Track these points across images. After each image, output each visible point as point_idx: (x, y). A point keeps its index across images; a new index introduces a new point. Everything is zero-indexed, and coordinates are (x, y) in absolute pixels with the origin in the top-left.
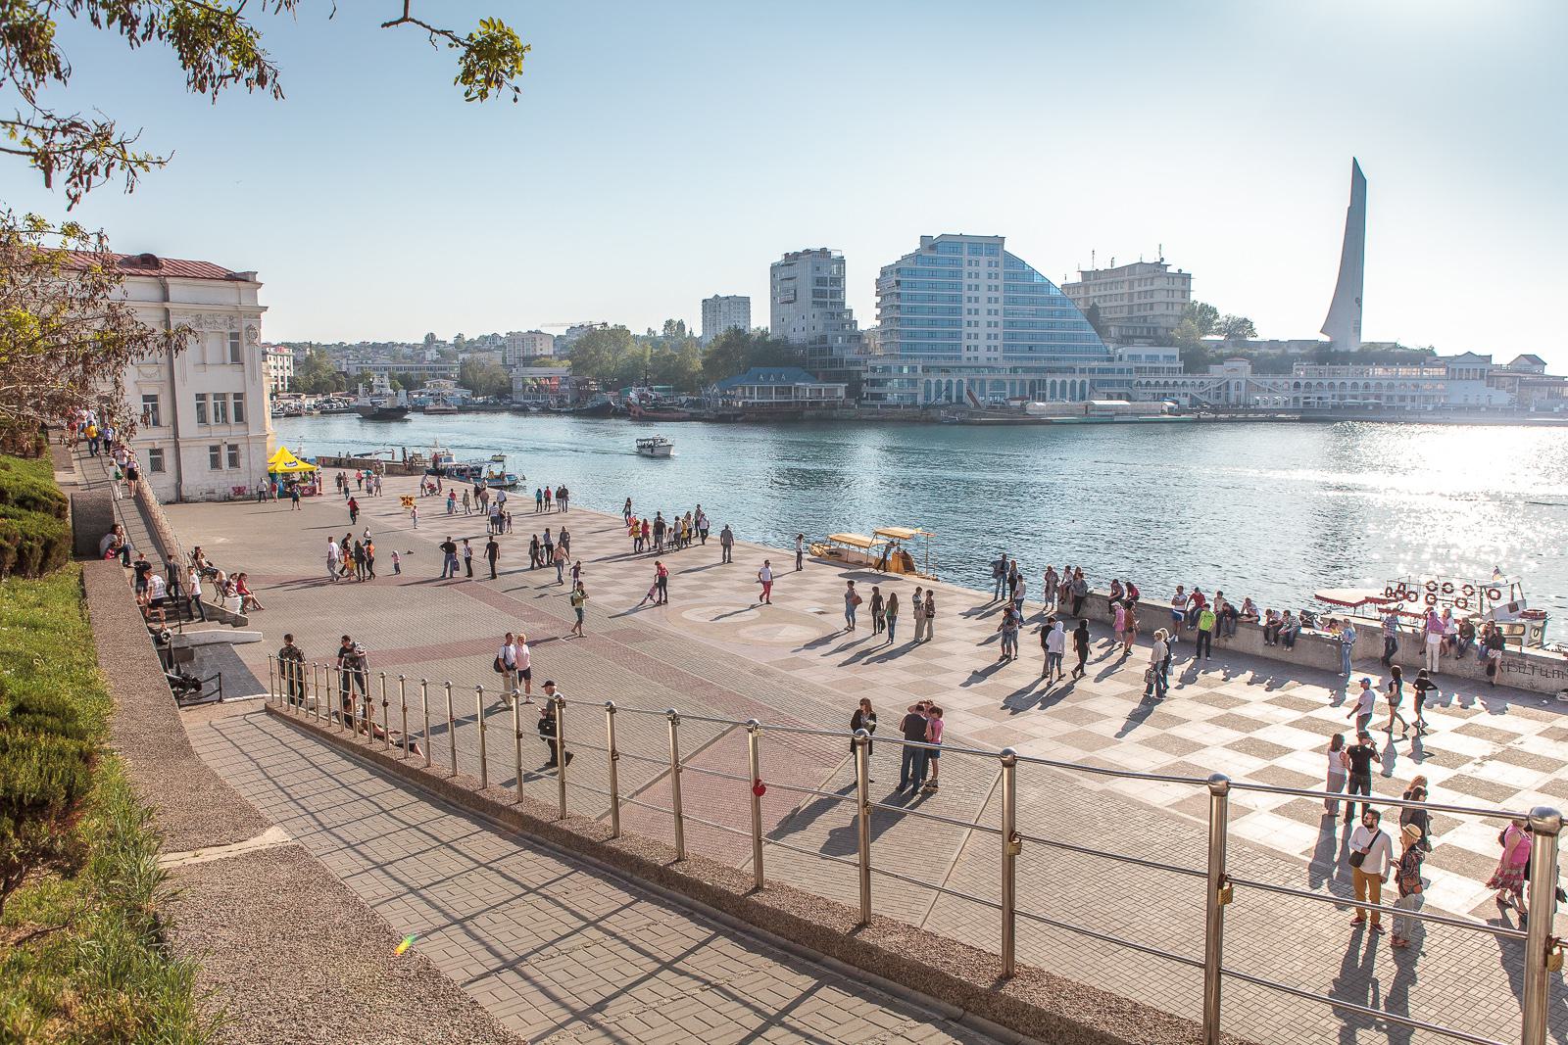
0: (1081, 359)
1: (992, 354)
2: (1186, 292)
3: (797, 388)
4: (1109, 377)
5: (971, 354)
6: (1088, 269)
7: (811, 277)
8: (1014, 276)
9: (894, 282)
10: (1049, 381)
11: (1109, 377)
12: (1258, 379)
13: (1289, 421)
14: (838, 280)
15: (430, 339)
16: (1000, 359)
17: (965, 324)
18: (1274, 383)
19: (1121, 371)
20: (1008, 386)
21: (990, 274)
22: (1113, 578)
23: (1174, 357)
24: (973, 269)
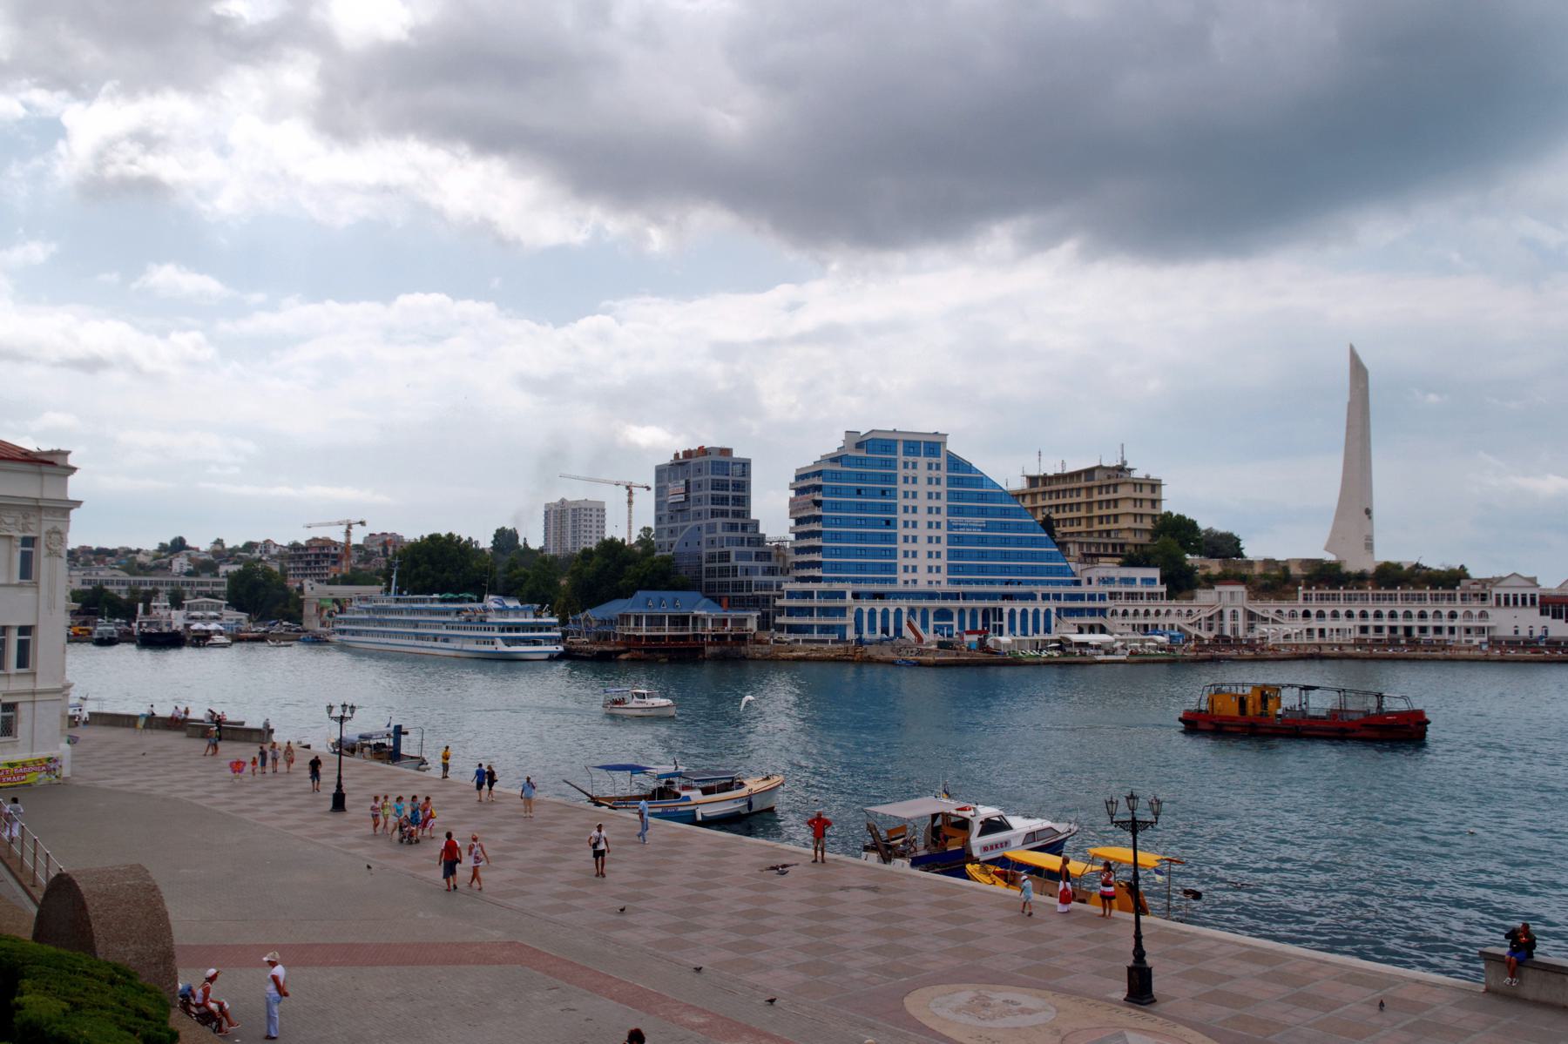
0: (1041, 582)
1: (934, 577)
2: (1155, 502)
3: (695, 618)
4: (1078, 604)
5: (910, 576)
6: (1035, 473)
7: (708, 481)
9: (810, 487)
10: (1006, 611)
11: (1078, 604)
12: (1258, 608)
13: (1427, 660)
14: (743, 486)
15: (179, 545)
18: (1279, 612)
19: (1092, 597)
20: (956, 617)
23: (1154, 580)
24: (910, 472)
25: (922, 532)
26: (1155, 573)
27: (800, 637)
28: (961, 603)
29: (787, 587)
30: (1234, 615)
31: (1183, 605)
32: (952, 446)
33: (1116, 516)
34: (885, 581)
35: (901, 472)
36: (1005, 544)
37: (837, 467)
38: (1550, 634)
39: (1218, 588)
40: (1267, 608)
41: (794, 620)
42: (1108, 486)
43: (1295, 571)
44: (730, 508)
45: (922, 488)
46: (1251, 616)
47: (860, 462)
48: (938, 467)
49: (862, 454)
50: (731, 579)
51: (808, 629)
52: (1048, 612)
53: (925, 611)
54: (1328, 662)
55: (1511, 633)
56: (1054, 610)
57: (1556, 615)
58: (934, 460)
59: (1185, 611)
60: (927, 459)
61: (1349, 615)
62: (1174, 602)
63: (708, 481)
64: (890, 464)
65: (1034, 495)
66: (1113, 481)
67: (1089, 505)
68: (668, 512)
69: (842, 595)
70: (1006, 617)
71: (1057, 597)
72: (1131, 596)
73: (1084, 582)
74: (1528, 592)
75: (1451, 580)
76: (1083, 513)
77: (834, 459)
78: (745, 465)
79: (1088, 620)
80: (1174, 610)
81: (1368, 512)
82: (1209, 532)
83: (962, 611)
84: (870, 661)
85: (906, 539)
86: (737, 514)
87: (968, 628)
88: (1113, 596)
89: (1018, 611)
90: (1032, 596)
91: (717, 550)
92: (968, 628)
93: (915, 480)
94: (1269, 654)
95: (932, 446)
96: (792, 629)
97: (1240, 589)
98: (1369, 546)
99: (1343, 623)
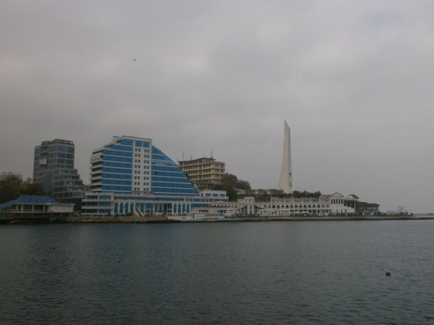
2: (222, 170)
4: (199, 203)
6: (181, 160)
10: (173, 204)
24: (138, 153)
25: (142, 175)
26: (224, 193)
27: (92, 214)
28: (156, 202)
29: (87, 194)
30: (251, 207)
31: (234, 204)
32: (155, 144)
33: (210, 175)
35: (134, 152)
36: (173, 181)
37: (109, 149)
38: (347, 212)
39: (245, 198)
40: (261, 205)
41: (90, 207)
42: (207, 165)
43: (268, 193)
44: (65, 164)
45: (142, 159)
46: (256, 207)
47: (119, 148)
48: (148, 151)
49: (119, 144)
50: (64, 192)
51: (95, 211)
52: (188, 205)
53: (142, 205)
54: (284, 222)
55: (336, 212)
56: (190, 205)
57: (349, 206)
58: (147, 149)
59: (234, 206)
60: (144, 148)
61: (287, 207)
62: (231, 203)
63: (56, 154)
64: (131, 149)
65: (181, 168)
66: (209, 163)
67: (200, 171)
69: (109, 197)
70: (173, 207)
71: (191, 200)
73: (201, 195)
74: (341, 198)
75: (316, 196)
76: (198, 174)
77: (110, 146)
79: (202, 209)
81: (290, 174)
82: (240, 181)
83: (156, 205)
84: (120, 222)
85: (135, 178)
86: (68, 167)
87: (158, 210)
89: (177, 204)
90: (182, 200)
91: (59, 181)
92: (158, 210)
93: (139, 156)
94: (264, 218)
95: (147, 144)
96: (89, 211)
97: (253, 198)
98: (291, 185)
99: (285, 209)
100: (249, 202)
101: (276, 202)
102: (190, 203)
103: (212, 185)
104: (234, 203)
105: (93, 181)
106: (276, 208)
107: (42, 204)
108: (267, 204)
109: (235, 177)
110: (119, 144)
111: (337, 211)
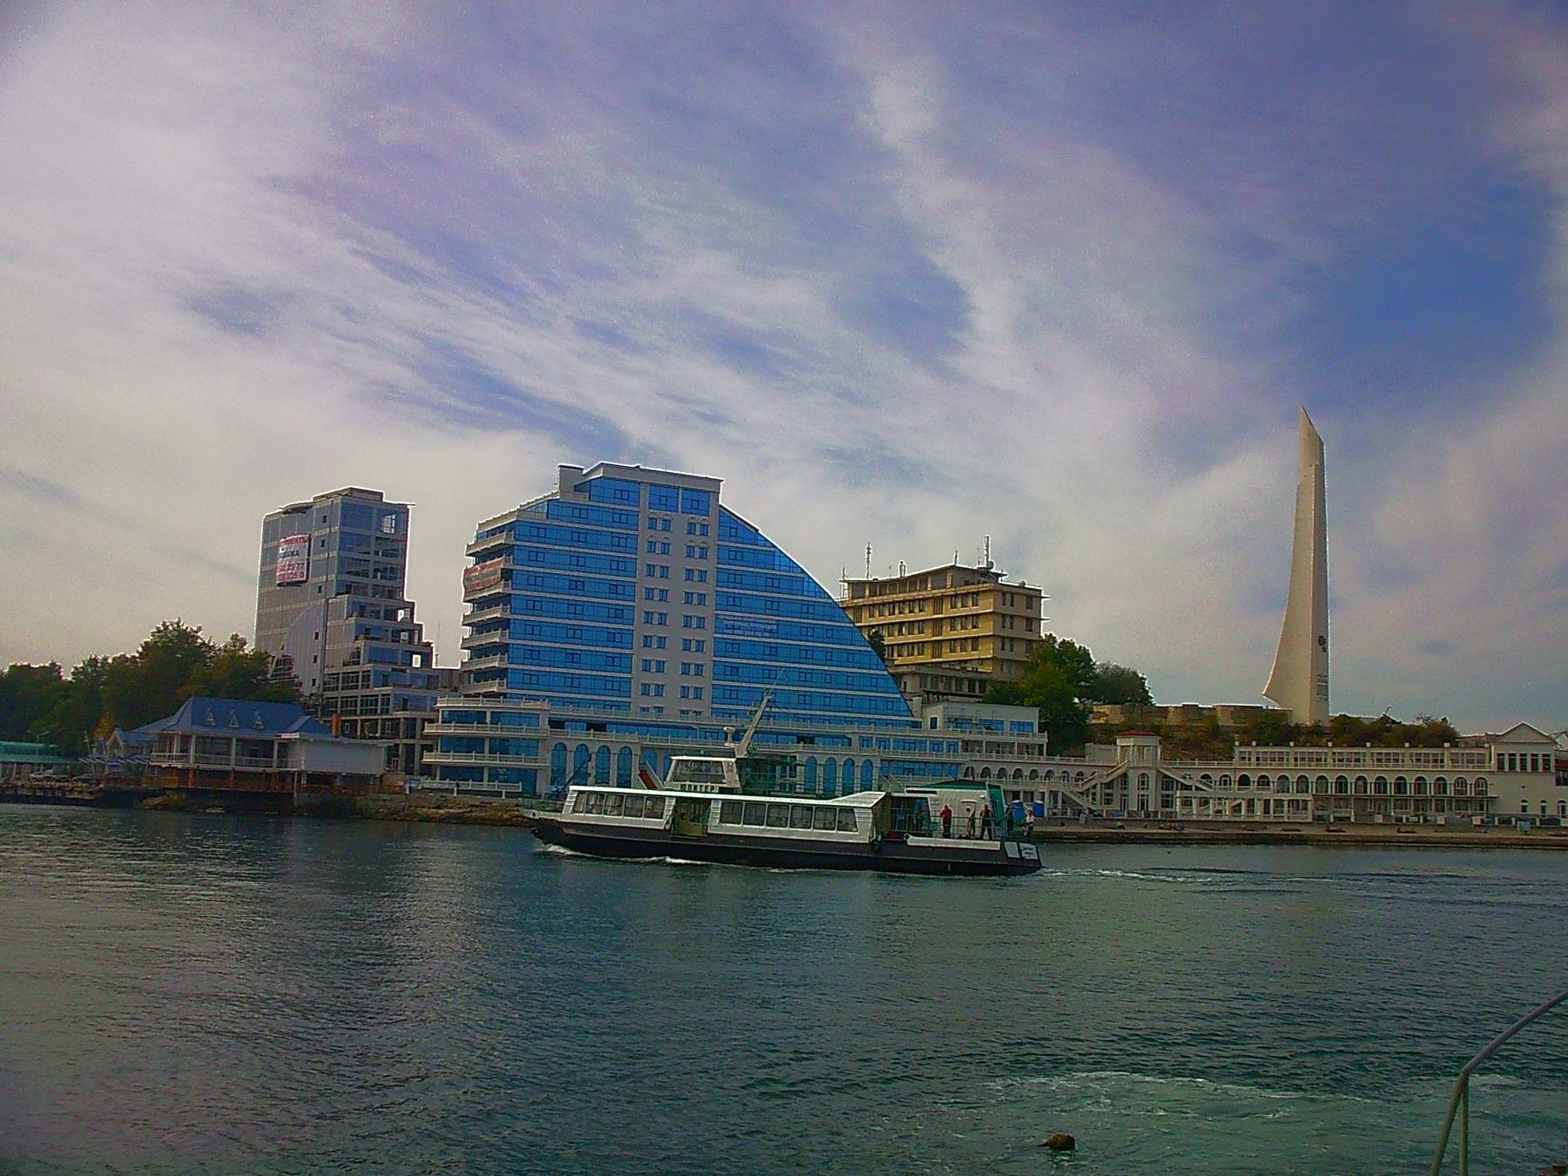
1: (691, 705)
2: (1033, 621)
8: (737, 556)
14: (395, 548)
16: (707, 713)
17: (638, 641)
21: (686, 666)
22: (499, 574)
26: (1031, 715)
30: (1143, 783)
31: (1072, 765)
34: (618, 706)
40: (1190, 772)
43: (1224, 721)
45: (678, 562)
49: (582, 499)
51: (474, 773)
59: (1073, 773)
65: (858, 609)
66: (972, 588)
68: (279, 589)
69: (533, 717)
72: (997, 747)
78: (401, 512)
80: (1058, 772)
82: (1106, 669)
88: (968, 746)
96: (450, 772)
97: (1153, 741)
100: (1130, 754)
101: (1249, 759)
102: (875, 754)
103: (983, 683)
104: (1072, 761)
105: (478, 652)
106: (1253, 787)
107: (267, 736)
108: (1216, 769)
109: (1084, 655)
110: (582, 499)
111: (1524, 809)
